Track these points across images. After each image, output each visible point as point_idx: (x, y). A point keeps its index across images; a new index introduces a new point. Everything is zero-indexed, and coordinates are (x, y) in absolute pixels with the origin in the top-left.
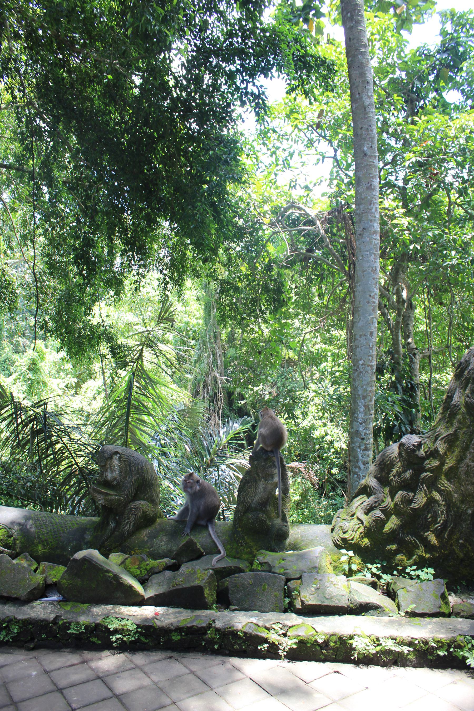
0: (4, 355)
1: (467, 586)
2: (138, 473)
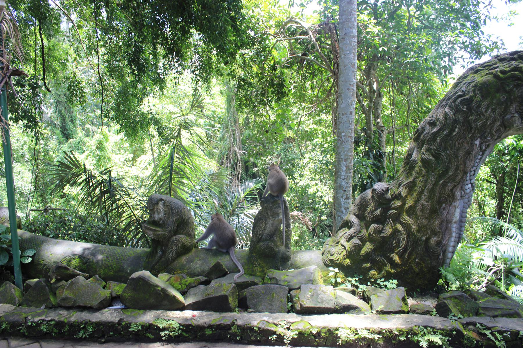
0: (78, 139)
1: (421, 292)
2: (178, 215)
